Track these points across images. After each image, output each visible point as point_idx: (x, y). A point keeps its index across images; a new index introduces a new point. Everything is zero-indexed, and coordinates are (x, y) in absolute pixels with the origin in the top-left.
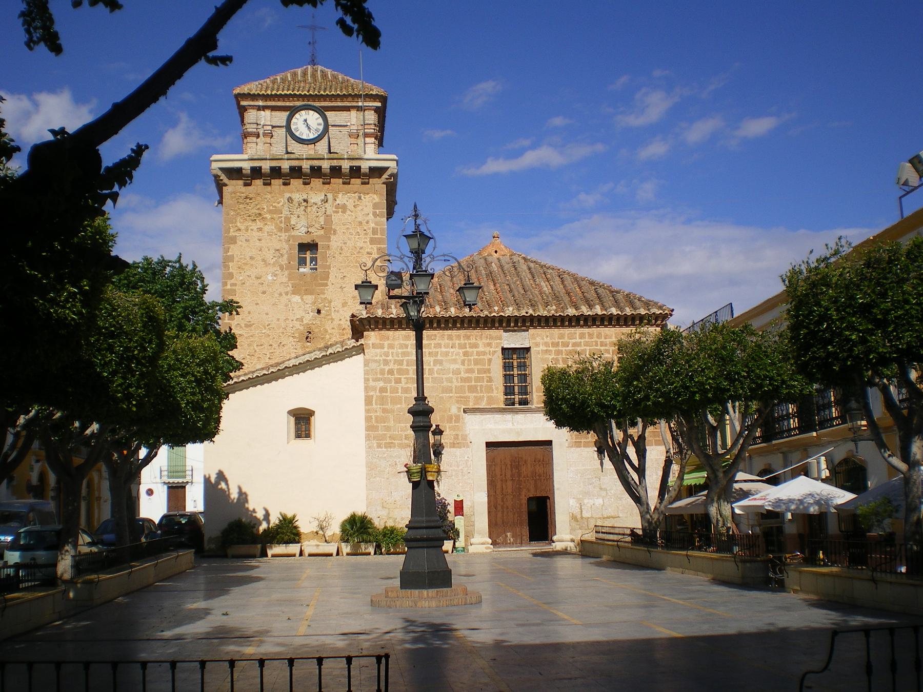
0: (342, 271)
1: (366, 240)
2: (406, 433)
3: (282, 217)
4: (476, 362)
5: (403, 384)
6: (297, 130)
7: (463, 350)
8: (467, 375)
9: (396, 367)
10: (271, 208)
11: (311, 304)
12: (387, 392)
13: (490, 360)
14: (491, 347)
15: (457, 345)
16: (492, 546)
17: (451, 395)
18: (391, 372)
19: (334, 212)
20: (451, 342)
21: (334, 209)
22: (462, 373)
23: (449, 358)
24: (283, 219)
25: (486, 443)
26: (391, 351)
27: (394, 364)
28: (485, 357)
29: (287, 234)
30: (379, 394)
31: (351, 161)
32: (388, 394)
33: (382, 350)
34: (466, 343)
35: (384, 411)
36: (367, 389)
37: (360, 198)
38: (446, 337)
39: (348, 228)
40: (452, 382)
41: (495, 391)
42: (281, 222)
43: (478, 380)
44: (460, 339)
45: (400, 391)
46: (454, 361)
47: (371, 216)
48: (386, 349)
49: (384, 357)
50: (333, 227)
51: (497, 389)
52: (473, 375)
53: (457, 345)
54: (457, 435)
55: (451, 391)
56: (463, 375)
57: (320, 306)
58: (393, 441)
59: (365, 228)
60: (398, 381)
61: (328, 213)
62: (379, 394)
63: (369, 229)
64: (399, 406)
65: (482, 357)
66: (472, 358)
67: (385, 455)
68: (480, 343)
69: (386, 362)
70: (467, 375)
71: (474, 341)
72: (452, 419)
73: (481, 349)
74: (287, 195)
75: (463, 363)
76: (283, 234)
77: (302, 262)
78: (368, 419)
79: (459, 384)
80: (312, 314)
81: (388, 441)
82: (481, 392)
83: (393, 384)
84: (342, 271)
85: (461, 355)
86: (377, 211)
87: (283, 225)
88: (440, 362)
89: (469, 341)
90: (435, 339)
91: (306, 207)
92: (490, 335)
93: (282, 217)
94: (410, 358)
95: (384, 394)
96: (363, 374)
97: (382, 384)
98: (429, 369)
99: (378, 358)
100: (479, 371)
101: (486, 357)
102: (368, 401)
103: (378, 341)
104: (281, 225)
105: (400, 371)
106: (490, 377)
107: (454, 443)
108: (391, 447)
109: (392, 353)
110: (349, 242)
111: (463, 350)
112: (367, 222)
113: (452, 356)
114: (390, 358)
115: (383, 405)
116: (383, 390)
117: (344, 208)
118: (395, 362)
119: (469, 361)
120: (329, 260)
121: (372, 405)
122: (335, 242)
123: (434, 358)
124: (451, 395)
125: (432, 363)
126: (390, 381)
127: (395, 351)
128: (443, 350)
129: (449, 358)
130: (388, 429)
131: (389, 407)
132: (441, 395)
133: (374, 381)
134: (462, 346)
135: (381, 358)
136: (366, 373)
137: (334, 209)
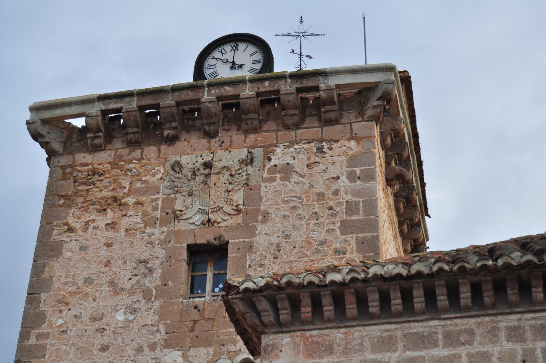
1: (332, 227)
3: (157, 199)
21: (265, 175)
24: (160, 202)
29: (165, 229)
38: (503, 335)
39: (294, 208)
42: (155, 209)
47: (344, 180)
50: (262, 208)
59: (331, 203)
61: (252, 183)
76: (157, 231)
86: (358, 170)
87: (158, 214)
90: (470, 343)
91: (207, 176)
93: (157, 199)
110: (294, 233)
137: (265, 175)
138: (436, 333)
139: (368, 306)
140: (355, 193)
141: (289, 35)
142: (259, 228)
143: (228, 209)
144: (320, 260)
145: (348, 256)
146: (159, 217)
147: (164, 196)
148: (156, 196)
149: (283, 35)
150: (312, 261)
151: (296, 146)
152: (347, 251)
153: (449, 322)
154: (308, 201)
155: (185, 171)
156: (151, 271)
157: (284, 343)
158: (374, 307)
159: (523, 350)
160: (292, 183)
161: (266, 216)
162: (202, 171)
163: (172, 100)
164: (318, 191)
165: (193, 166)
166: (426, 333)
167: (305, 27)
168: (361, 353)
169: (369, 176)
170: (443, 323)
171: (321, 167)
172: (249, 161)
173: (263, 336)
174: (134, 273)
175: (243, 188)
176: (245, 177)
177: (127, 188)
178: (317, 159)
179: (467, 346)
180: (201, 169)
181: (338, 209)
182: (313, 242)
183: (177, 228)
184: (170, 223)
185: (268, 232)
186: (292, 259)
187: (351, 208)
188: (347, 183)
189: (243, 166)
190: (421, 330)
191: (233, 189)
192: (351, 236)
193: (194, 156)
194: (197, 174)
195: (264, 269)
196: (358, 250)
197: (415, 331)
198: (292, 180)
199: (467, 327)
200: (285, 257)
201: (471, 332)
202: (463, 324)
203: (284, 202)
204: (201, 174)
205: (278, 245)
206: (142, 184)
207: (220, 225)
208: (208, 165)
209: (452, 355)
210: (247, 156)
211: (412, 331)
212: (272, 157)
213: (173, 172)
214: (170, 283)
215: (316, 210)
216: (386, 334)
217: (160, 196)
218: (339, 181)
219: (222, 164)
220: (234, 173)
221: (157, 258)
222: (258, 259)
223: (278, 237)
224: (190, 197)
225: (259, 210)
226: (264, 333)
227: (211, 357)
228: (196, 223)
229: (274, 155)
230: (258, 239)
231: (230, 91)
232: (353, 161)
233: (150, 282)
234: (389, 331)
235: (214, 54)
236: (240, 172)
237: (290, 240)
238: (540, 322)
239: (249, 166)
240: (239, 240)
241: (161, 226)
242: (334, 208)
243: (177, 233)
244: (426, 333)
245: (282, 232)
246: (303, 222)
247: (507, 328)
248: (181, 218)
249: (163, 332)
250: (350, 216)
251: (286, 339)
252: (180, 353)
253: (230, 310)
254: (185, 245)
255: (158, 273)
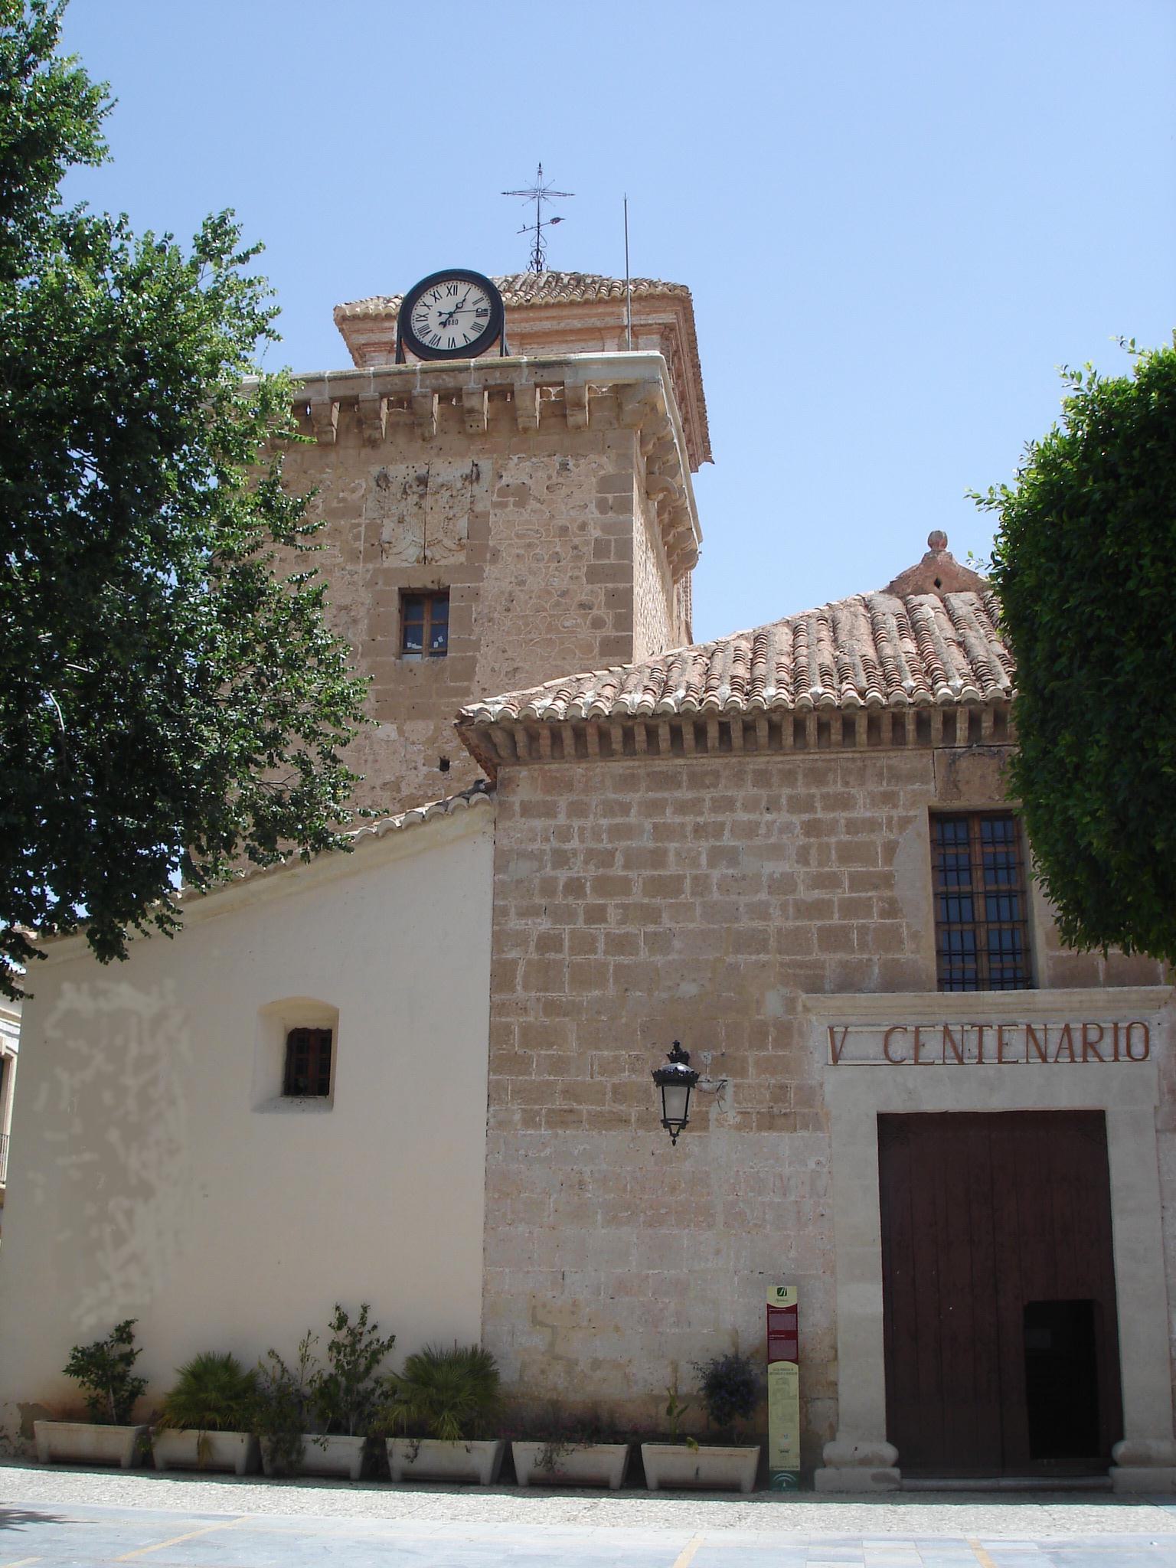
0: (509, 654)
1: (576, 573)
2: (615, 1080)
3: (359, 525)
4: (847, 854)
5: (612, 924)
6: (426, 330)
7: (806, 817)
8: (817, 894)
9: (592, 871)
10: (335, 504)
11: (423, 744)
12: (559, 950)
13: (891, 849)
14: (895, 806)
15: (784, 801)
16: (896, 1472)
17: (764, 957)
18: (575, 887)
19: (495, 505)
20: (763, 793)
21: (495, 498)
22: (801, 888)
23: (758, 841)
24: (362, 529)
25: (883, 1119)
26: (576, 823)
27: (586, 862)
28: (873, 837)
29: (370, 566)
30: (535, 956)
31: (540, 372)
32: (565, 955)
33: (553, 822)
34: (813, 796)
35: (551, 1008)
36: (499, 939)
37: (564, 466)
38: (749, 777)
39: (529, 545)
40: (765, 916)
41: (908, 945)
42: (357, 538)
43: (850, 908)
44: (792, 784)
45: (601, 945)
46: (776, 851)
47: (593, 513)
48: (562, 819)
49: (555, 843)
50: (491, 543)
51: (915, 936)
52: (837, 896)
53: (784, 801)
54: (783, 1088)
55: (763, 948)
56: (803, 894)
57: (447, 747)
58: (575, 1106)
59: (576, 541)
60: (596, 915)
61: (479, 508)
62: (535, 956)
63: (587, 543)
64: (596, 993)
65: (863, 837)
66: (833, 840)
67: (548, 1151)
68: (859, 794)
69: (561, 859)
70: (817, 894)
71: (839, 788)
72: (766, 1035)
73: (861, 813)
74: (375, 470)
75: (803, 857)
76: (360, 567)
77: (408, 634)
78: (498, 1035)
79: (790, 924)
80: (424, 770)
81: (559, 1104)
82: (863, 946)
83: (580, 924)
84: (509, 654)
85: (798, 830)
86: (610, 496)
87: (361, 545)
88: (731, 856)
89: (825, 790)
90: (715, 786)
91: (422, 496)
92: (890, 768)
93: (359, 525)
94: (634, 844)
95: (552, 956)
96: (490, 897)
97: (544, 924)
98: (695, 878)
99: (535, 846)
100: (857, 882)
101: (880, 838)
102: (501, 977)
103: (539, 796)
104: (356, 545)
105: (603, 886)
106: (892, 902)
107: (772, 1116)
108: (564, 1124)
109: (582, 830)
110: (530, 579)
111: (806, 817)
112: (583, 527)
113: (768, 835)
114: (574, 843)
115: (546, 990)
116: (548, 943)
117: (521, 494)
118: (590, 854)
119: (823, 849)
120: (477, 629)
121: (513, 990)
122: (495, 580)
123: (712, 842)
124: (764, 957)
125: (704, 860)
126: (570, 915)
127: (589, 823)
128: (743, 816)
129: (758, 841)
130: (559, 1065)
131: (565, 995)
132: (730, 959)
133: (522, 914)
134: (798, 805)
135: (547, 847)
136: (499, 890)
137: (495, 498)
138: (680, 773)
139: (611, 743)
140: (607, 528)
141: (521, 193)
142: (487, 570)
143: (448, 543)
144: (561, 615)
145: (595, 611)
146: (362, 549)
147: (368, 521)
148: (356, 521)
149: (514, 193)
150: (551, 616)
151: (534, 460)
152: (593, 605)
153: (695, 762)
154: (547, 536)
155: (393, 488)
156: (355, 621)
157: (521, 776)
158: (617, 746)
159: (769, 796)
160: (529, 511)
161: (495, 555)
162: (415, 488)
163: (375, 392)
164: (560, 524)
165: (404, 481)
166: (670, 773)
167: (545, 182)
168: (602, 791)
169: (625, 507)
170: (689, 762)
171: (564, 491)
172: (474, 477)
173: (499, 768)
174: (334, 623)
175: (467, 516)
176: (469, 500)
177: (320, 508)
178: (560, 480)
179: (712, 789)
180: (414, 486)
181: (585, 549)
182: (553, 591)
183: (386, 565)
184: (376, 558)
185: (498, 576)
186: (527, 613)
187: (601, 549)
188: (596, 514)
189: (467, 483)
190: (665, 769)
191: (454, 516)
192: (599, 585)
193: (404, 467)
194: (409, 492)
195: (494, 625)
196: (608, 605)
197: (659, 769)
198: (529, 508)
199: (713, 767)
200: (519, 609)
201: (716, 774)
202: (709, 765)
203: (518, 536)
204: (413, 493)
205: (510, 594)
206: (339, 502)
207: (438, 564)
208: (423, 481)
209: (695, 798)
210: (472, 471)
211: (655, 769)
212: (504, 474)
213: (379, 488)
214: (379, 638)
215: (557, 549)
216: (629, 771)
217: (362, 520)
218: (587, 510)
219: (440, 480)
220: (454, 494)
221: (362, 604)
222: (486, 611)
223: (511, 583)
224: (402, 525)
225: (487, 546)
226: (500, 765)
227: (431, 732)
228: (410, 560)
229: (505, 470)
230: (486, 585)
231: (450, 382)
232: (605, 484)
233: (355, 635)
234: (633, 768)
235: (424, 299)
236: (463, 491)
237: (525, 588)
238: (788, 767)
239: (475, 484)
240: (463, 585)
241: (365, 561)
242: (580, 548)
243: (387, 572)
244: (670, 773)
245: (516, 577)
246: (541, 565)
247: (754, 771)
248: (391, 551)
249: (373, 700)
250: (598, 559)
251: (524, 773)
252: (395, 727)
253: (465, 740)
254: (397, 588)
255: (363, 625)
